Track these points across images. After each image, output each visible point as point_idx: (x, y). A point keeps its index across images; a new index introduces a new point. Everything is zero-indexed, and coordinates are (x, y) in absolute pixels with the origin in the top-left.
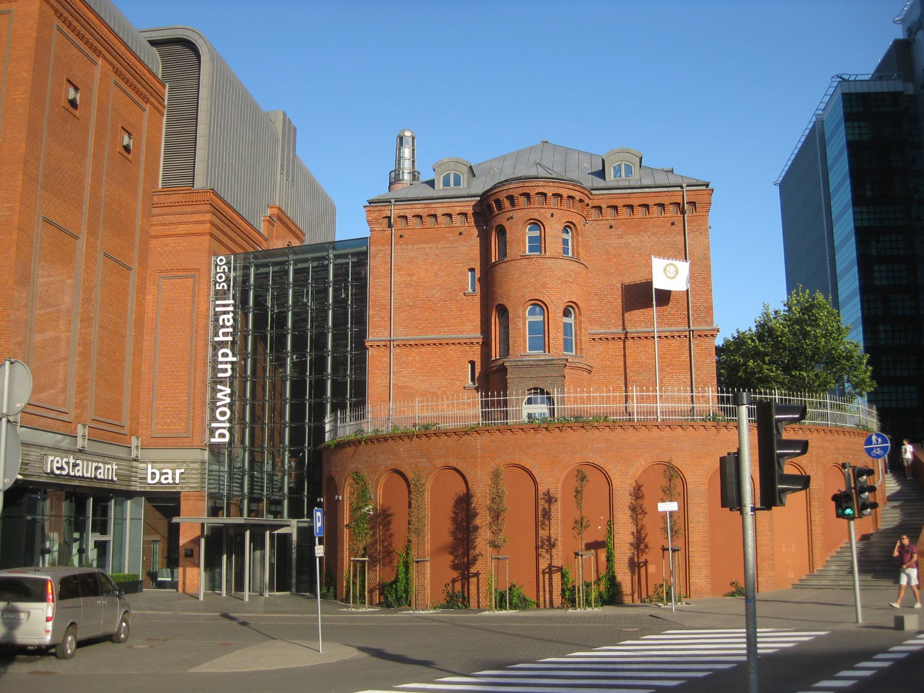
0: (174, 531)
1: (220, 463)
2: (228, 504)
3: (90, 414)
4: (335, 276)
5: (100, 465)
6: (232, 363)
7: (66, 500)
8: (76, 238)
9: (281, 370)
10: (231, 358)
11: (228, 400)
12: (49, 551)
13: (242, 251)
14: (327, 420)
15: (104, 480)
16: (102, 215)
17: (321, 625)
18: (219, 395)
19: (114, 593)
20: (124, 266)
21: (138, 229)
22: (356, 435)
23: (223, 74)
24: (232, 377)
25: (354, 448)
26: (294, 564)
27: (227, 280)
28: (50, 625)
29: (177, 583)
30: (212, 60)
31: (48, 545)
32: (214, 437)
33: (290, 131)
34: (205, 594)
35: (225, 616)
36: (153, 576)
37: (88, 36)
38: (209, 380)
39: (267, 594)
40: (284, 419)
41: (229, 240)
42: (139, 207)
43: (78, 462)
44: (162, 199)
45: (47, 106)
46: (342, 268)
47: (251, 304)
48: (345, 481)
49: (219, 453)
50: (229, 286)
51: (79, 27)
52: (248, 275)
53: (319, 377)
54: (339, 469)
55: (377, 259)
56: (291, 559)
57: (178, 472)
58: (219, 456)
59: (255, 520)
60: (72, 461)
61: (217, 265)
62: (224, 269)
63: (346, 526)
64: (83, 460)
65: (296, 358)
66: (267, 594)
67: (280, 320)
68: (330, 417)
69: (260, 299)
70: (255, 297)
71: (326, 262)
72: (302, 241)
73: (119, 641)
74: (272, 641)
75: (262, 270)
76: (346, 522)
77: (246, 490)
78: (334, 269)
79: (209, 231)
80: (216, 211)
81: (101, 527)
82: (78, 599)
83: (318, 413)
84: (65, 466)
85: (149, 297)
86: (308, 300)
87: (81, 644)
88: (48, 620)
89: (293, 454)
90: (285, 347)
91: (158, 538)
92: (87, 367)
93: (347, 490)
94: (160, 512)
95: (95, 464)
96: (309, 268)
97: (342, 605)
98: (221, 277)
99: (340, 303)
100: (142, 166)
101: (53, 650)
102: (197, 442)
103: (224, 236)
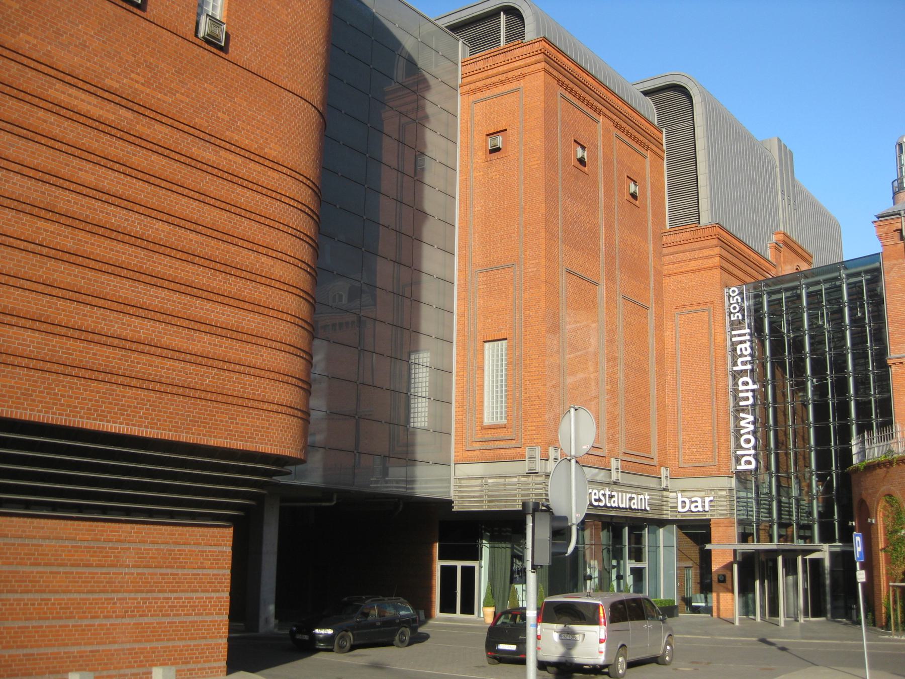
0: (706, 558)
1: (747, 489)
2: (758, 530)
3: (622, 448)
4: (849, 295)
5: (634, 495)
6: (753, 391)
7: (603, 530)
8: (596, 284)
9: (800, 394)
10: (751, 386)
11: (751, 427)
12: (590, 578)
13: (753, 281)
14: (853, 442)
15: (638, 510)
16: (617, 261)
17: (868, 653)
18: (742, 423)
19: (657, 617)
20: (642, 306)
21: (651, 269)
22: (886, 457)
23: (716, 113)
24: (754, 405)
25: (885, 469)
26: (828, 589)
27: (742, 310)
28: (603, 646)
29: (711, 608)
30: (704, 100)
31: (588, 571)
32: (740, 465)
33: (787, 156)
34: (740, 619)
35: (763, 641)
36: (687, 601)
37: (588, 98)
38: (731, 409)
39: (802, 619)
40: (809, 443)
41: (739, 271)
42: (651, 247)
43: (613, 493)
44: (671, 239)
45: (560, 167)
46: (855, 287)
47: (767, 331)
48: (878, 503)
49: (746, 480)
50: (743, 316)
51: (579, 91)
52: (762, 303)
53: (841, 398)
54: (870, 491)
55: (892, 274)
56: (824, 585)
57: (707, 500)
58: (746, 483)
59: (788, 546)
60: (608, 493)
61: (729, 296)
62: (737, 299)
63: (881, 550)
64: (616, 491)
65: (817, 381)
66: (802, 619)
67: (797, 345)
68: (857, 439)
69: (774, 325)
70: (771, 323)
71: (838, 283)
72: (810, 263)
73: (664, 663)
74: (814, 667)
75: (774, 297)
76: (881, 545)
77: (775, 516)
78: (848, 289)
79: (719, 264)
80: (723, 243)
81: (637, 555)
82: (626, 622)
83: (844, 436)
84: (602, 498)
85: (667, 334)
86: (824, 322)
87: (631, 665)
88: (601, 641)
89: (821, 478)
90: (805, 371)
91: (690, 564)
92: (616, 404)
93: (880, 515)
94: (691, 539)
95: (629, 495)
96: (821, 290)
97: (882, 632)
98: (735, 308)
99: (857, 322)
100: (649, 210)
101: (606, 670)
102: (723, 470)
103: (733, 267)
